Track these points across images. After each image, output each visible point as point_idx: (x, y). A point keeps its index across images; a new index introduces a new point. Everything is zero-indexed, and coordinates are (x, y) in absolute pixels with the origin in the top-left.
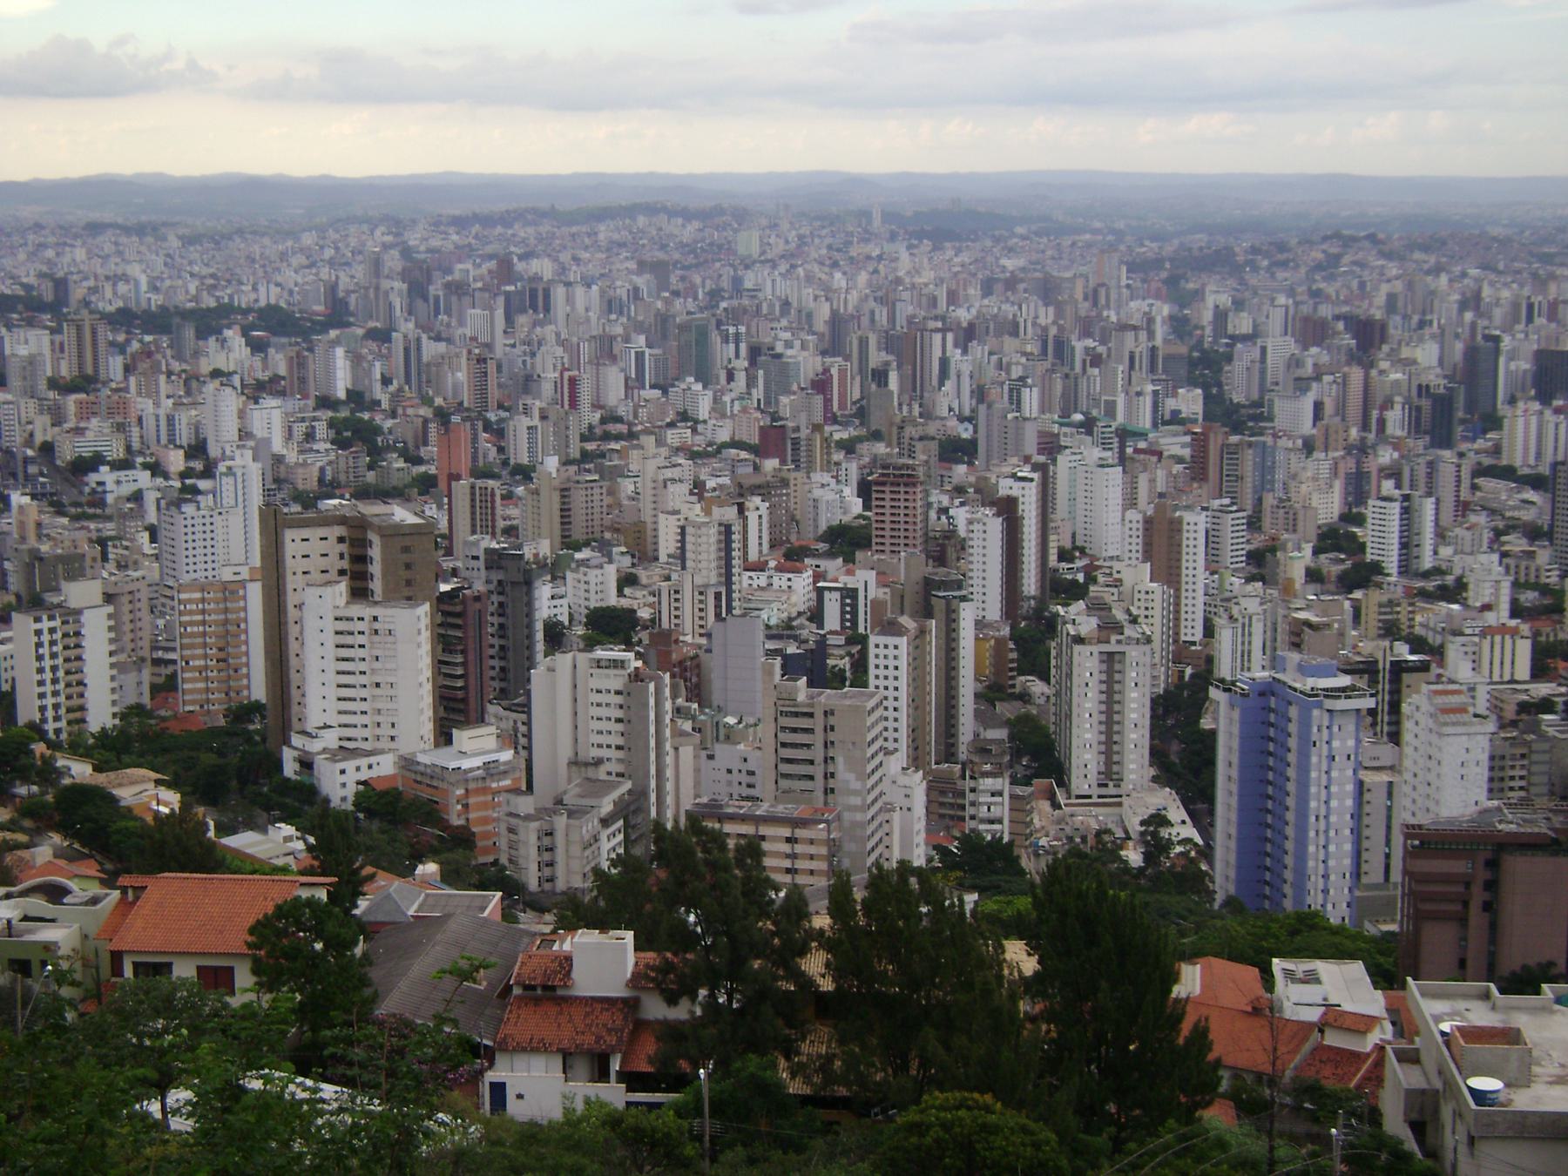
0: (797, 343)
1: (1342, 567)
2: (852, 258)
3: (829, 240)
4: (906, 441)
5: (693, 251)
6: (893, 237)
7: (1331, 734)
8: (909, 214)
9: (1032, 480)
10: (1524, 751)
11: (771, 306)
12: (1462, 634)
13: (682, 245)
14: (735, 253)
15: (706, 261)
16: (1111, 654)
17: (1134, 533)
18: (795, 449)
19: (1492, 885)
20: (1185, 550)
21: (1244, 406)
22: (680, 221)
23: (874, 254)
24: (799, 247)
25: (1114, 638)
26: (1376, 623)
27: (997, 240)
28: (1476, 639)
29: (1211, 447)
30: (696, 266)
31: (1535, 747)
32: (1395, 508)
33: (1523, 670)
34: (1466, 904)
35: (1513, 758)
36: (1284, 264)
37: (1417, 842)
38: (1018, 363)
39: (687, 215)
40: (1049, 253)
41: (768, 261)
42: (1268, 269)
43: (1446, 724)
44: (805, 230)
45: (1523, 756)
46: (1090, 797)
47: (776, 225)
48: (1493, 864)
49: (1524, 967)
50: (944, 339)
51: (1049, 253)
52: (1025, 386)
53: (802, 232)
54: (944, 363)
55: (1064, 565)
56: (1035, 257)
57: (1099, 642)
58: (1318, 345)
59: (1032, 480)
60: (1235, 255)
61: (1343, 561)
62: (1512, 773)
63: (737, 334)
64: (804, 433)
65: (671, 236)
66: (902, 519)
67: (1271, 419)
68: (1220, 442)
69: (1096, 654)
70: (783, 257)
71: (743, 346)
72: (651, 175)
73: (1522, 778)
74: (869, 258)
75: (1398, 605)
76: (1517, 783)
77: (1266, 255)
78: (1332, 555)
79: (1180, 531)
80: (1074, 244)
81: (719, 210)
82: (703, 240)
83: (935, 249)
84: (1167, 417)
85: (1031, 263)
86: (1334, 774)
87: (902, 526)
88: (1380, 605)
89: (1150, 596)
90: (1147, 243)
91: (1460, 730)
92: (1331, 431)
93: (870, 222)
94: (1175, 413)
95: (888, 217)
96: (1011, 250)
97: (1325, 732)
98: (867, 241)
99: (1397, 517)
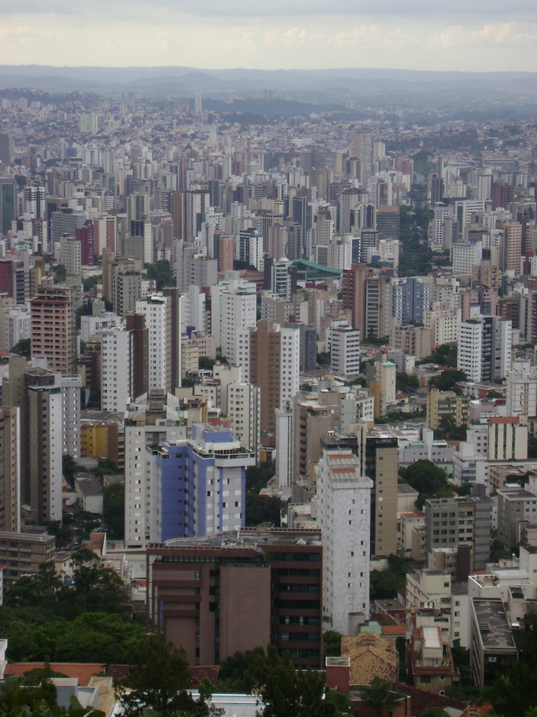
0: (89, 202)
1: (434, 375)
2: (171, 136)
3: (157, 123)
4: (116, 275)
5: (46, 129)
6: (210, 120)
7: (221, 486)
8: (230, 102)
9: (161, 302)
10: (471, 509)
11: (86, 172)
12: (478, 423)
13: (38, 123)
14: (78, 131)
15: (54, 137)
16: (156, 434)
17: (244, 345)
18: (20, 280)
19: (214, 590)
20: (282, 358)
21: (439, 254)
22: (39, 104)
23: (189, 134)
24: (132, 126)
25: (158, 421)
26: (436, 417)
27: (292, 123)
28: (486, 427)
29: (357, 282)
30: (45, 140)
31: (478, 506)
32: (479, 329)
33: (522, 451)
34: (198, 605)
35: (462, 514)
36: (515, 144)
37: (160, 557)
38: (249, 218)
39: (45, 99)
40: (332, 134)
41: (104, 137)
42: (502, 147)
43: (336, 480)
44: (140, 114)
45: (470, 514)
46: (140, 546)
47: (117, 109)
48: (215, 574)
49: (238, 654)
50: (203, 200)
51: (332, 134)
52: (253, 236)
53: (137, 114)
54: (201, 218)
55: (203, 371)
56: (321, 137)
57: (147, 424)
58: (502, 206)
59: (161, 302)
60: (477, 136)
61: (436, 370)
62: (461, 527)
63: (38, 193)
64: (29, 267)
65: (30, 116)
66: (54, 332)
67: (451, 264)
68: (363, 278)
69: (143, 434)
70: (116, 134)
71: (43, 203)
72: (33, 67)
73: (469, 531)
74: (185, 136)
75: (455, 402)
76: (466, 535)
77: (502, 136)
78: (427, 366)
79: (279, 343)
80: (352, 127)
81: (74, 96)
82: (55, 120)
83: (243, 129)
84: (369, 261)
85: (317, 142)
86: (225, 517)
87: (54, 338)
88: (440, 402)
89: (240, 393)
90: (415, 127)
91: (348, 485)
92: (482, 272)
93: (192, 107)
94: (375, 258)
95: (207, 103)
96: (302, 131)
97: (217, 484)
98: (189, 123)
99: (480, 335)
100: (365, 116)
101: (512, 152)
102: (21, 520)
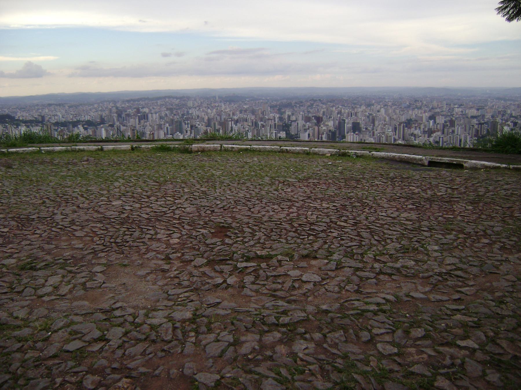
6: (221, 102)
13: (176, 105)
27: (243, 102)
36: (302, 106)
39: (177, 98)
42: (299, 107)
72: (169, 90)
74: (216, 106)
81: (183, 97)
83: (230, 104)
95: (219, 97)
100: (260, 100)
101: (301, 108)
102: (481, 165)
